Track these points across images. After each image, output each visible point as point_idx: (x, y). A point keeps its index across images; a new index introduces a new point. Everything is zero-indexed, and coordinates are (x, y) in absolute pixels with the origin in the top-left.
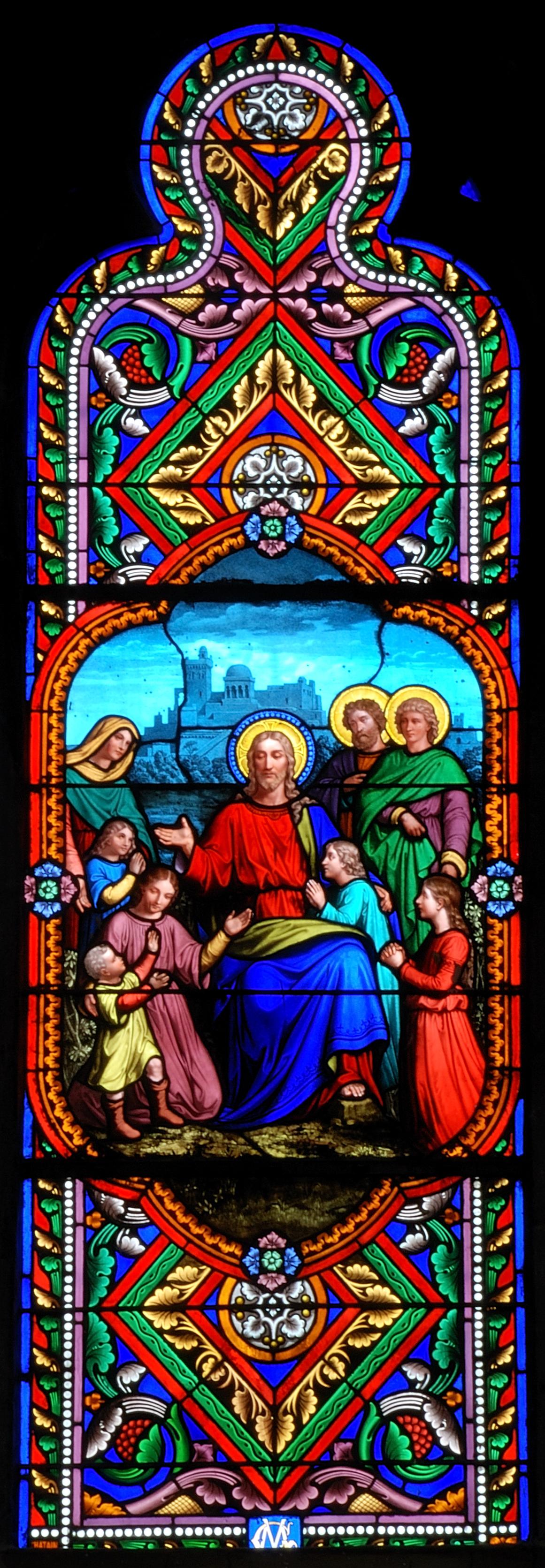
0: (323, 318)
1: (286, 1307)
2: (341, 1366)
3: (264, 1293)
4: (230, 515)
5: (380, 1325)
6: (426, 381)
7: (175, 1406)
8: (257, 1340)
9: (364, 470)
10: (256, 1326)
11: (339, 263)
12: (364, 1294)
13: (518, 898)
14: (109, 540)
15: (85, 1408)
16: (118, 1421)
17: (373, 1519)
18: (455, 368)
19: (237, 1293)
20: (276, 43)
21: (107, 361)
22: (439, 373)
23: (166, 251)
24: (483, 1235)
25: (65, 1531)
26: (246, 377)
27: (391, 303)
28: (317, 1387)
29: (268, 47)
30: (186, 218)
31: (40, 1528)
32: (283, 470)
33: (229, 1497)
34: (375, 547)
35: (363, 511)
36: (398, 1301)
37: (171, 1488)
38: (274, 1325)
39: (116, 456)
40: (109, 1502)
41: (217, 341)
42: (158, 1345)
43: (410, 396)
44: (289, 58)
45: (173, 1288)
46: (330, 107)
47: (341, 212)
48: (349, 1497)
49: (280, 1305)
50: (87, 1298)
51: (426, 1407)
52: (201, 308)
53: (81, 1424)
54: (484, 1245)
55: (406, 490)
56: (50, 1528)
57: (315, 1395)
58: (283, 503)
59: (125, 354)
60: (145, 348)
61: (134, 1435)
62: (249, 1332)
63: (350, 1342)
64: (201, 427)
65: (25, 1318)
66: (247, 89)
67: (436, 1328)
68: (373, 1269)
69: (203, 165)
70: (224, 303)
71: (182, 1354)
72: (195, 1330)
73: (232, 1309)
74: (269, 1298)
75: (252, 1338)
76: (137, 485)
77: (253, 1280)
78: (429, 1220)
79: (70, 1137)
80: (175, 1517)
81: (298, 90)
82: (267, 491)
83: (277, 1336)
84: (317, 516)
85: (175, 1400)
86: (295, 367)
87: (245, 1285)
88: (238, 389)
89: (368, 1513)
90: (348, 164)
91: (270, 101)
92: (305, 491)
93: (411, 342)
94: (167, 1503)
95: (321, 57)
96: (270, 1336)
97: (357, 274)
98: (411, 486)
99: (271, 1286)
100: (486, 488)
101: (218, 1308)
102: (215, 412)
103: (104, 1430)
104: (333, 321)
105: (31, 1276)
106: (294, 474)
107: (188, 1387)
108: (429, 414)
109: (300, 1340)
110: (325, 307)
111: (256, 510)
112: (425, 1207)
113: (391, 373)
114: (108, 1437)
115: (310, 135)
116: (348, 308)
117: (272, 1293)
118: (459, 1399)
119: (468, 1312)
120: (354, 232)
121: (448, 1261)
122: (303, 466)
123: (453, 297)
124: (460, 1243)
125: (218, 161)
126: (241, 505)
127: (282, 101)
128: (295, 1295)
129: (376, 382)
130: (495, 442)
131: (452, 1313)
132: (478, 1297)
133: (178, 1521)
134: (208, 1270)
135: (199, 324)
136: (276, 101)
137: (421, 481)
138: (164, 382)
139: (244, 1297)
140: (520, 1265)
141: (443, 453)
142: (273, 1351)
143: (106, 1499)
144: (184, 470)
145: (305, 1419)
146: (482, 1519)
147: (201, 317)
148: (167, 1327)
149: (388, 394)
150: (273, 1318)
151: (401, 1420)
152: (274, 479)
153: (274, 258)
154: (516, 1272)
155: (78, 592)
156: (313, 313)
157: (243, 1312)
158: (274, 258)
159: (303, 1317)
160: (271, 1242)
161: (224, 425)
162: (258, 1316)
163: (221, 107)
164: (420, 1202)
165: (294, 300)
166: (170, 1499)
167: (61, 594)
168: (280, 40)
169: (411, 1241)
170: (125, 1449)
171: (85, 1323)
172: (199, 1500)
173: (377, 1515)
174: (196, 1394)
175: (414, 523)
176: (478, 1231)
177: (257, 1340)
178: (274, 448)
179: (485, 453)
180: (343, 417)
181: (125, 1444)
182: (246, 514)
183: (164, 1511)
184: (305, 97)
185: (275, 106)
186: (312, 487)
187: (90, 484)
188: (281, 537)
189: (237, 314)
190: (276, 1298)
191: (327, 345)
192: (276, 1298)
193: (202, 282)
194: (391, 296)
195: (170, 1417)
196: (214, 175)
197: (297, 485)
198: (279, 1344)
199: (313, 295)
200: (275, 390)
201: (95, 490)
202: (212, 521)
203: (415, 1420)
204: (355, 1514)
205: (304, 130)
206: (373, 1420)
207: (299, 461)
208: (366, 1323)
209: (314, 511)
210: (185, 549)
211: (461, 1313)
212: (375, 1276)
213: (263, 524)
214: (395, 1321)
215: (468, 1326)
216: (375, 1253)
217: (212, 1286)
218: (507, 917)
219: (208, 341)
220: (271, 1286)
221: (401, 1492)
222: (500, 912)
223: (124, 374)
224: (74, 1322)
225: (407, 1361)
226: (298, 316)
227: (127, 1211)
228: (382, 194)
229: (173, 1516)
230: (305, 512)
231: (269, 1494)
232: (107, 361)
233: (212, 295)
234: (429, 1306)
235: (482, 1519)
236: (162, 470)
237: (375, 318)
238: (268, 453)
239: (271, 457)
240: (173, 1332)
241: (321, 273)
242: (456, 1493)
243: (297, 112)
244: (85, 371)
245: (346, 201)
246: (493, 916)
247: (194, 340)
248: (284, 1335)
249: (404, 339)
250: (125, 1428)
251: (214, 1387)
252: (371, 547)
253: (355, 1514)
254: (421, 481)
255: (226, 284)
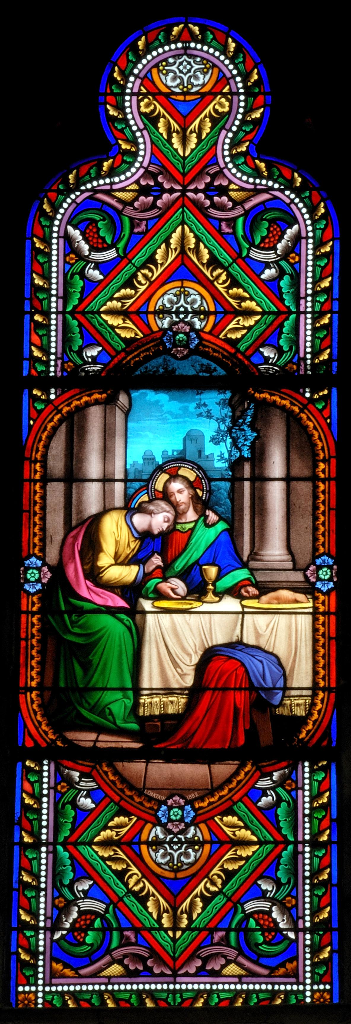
0: (214, 205)
1: (174, 312)
2: (140, 278)
3: (170, 834)
4: (153, 332)
5: (115, 302)
6: (279, 246)
7: (111, 907)
8: (164, 864)
9: (115, 854)
10: (164, 856)
11: (225, 171)
12: (234, 835)
13: (335, 580)
14: (76, 348)
15: (54, 906)
16: (75, 915)
17: (236, 980)
18: (297, 238)
19: (153, 834)
20: (186, 29)
21: (76, 233)
22: (288, 241)
23: (113, 163)
24: (310, 796)
25: (40, 988)
26: (194, 918)
27: (257, 196)
28: (202, 896)
29: (181, 33)
30: (127, 141)
31: (24, 986)
32: (195, 72)
33: (145, 965)
34: (109, 800)
35: (237, 329)
36: (103, 316)
37: (107, 959)
38: (176, 855)
39: (82, 293)
40: (67, 968)
41: (147, 220)
42: (100, 866)
43: (269, 256)
44: (194, 38)
45: (112, 831)
46: (220, 70)
47: (226, 137)
48: (221, 965)
49: (177, 313)
50: (297, 321)
51: (87, 253)
52: (136, 199)
53: (51, 918)
54: (311, 802)
55: (266, 316)
56: (31, 985)
57: (201, 901)
58: (170, 832)
59: (88, 229)
60: (100, 224)
61: (270, 238)
62: (160, 860)
63: (133, 292)
64: (135, 276)
65: (16, 849)
66: (166, 60)
67: (280, 856)
68: (240, 819)
69: (139, 107)
70: (151, 195)
71: (115, 872)
72: (125, 857)
73: (149, 844)
74: (173, 838)
75: (161, 863)
76: (93, 313)
77: (164, 826)
78: (277, 787)
79: (46, 733)
80: (112, 982)
81: (198, 59)
82: (180, 839)
83: (178, 863)
84: (210, 333)
85: (112, 902)
86: (196, 236)
87: (158, 828)
88: (199, 911)
89: (233, 976)
90: (231, 107)
91: (181, 68)
92: (202, 317)
93: (84, 943)
94: (105, 969)
95: (214, 38)
96: (173, 863)
97: (237, 178)
98: (270, 313)
99: (175, 830)
100: (317, 316)
101: (140, 843)
102: (215, 894)
103: (66, 921)
104: (221, 208)
105: (20, 823)
106: (196, 306)
107: (121, 895)
108: (280, 267)
109: (192, 865)
110: (216, 199)
111: (188, 826)
112: (274, 778)
113: (257, 241)
114: (285, 236)
115: (206, 89)
116: (230, 199)
117: (175, 835)
118: (68, 259)
119: (300, 847)
120: (234, 152)
121: (288, 814)
122: (201, 300)
123: (298, 191)
124: (295, 801)
125: (148, 105)
126: (160, 325)
127: (189, 67)
128: (189, 836)
129: (107, 915)
130: (323, 286)
131: (290, 847)
132: (307, 837)
133: (113, 980)
134: (135, 819)
135: (225, 957)
136: (185, 67)
137: (276, 310)
138: (113, 245)
139: (157, 836)
140: (334, 816)
141: (65, 866)
142: (176, 871)
143: (66, 966)
144: (236, 854)
145: (195, 917)
146: (308, 981)
147: (136, 204)
148: (248, 302)
149: (256, 255)
150: (176, 851)
151: (256, 916)
152: (175, 847)
153: (184, 168)
154: (332, 820)
155: (55, 382)
156: (149, 963)
157: (156, 846)
158: (184, 168)
159: (195, 851)
160: (175, 801)
161: (208, 885)
162: (166, 850)
163: (150, 71)
164: (271, 775)
165: (196, 194)
166: (109, 964)
167: (45, 383)
168: (189, 28)
169: (264, 801)
170: (275, 229)
171: (55, 853)
172: (126, 967)
173: (240, 977)
174: (125, 899)
175: (270, 337)
176: (307, 793)
177: (164, 864)
178: (182, 290)
179: (315, 294)
180: (225, 269)
181: (275, 233)
182: (194, 822)
183: (105, 973)
184: (203, 64)
185: (185, 71)
186: (207, 314)
187: (296, 843)
188: (170, 808)
189: (159, 203)
190: (178, 838)
191: (216, 223)
192: (178, 838)
193: (137, 182)
194: (257, 192)
195: (108, 913)
196: (145, 115)
197: (196, 313)
198: (178, 867)
199: (209, 190)
200: (184, 130)
201: (291, 839)
202: (216, 818)
203: (266, 917)
204: (225, 976)
205: (204, 85)
206: (121, 245)
207: (198, 298)
208: (123, 303)
209: (208, 329)
210: (236, 798)
211: (296, 848)
212: (241, 824)
213: (182, 816)
214: (254, 853)
215: (300, 856)
216: (241, 808)
217: (137, 830)
218: (29, 557)
219: (141, 220)
220: (175, 830)
221: (256, 963)
222: (33, 559)
223: (87, 242)
224: (47, 852)
225: (260, 877)
226: (197, 204)
227: (80, 781)
228: (251, 127)
229: (109, 977)
230: (202, 330)
231: (171, 963)
232: (76, 233)
233: (144, 191)
234: (276, 843)
235: (308, 981)
236: (250, 854)
237: (248, 206)
238: (178, 293)
239: (180, 295)
240: (244, 299)
241: (214, 177)
242: (292, 963)
243: (198, 73)
244: (62, 241)
245: (230, 130)
246: (38, 558)
247: (131, 219)
248: (182, 862)
249: (89, 945)
250: (79, 920)
251: (136, 894)
252: (112, 801)
253: (225, 976)
254: (276, 310)
255: (152, 183)
